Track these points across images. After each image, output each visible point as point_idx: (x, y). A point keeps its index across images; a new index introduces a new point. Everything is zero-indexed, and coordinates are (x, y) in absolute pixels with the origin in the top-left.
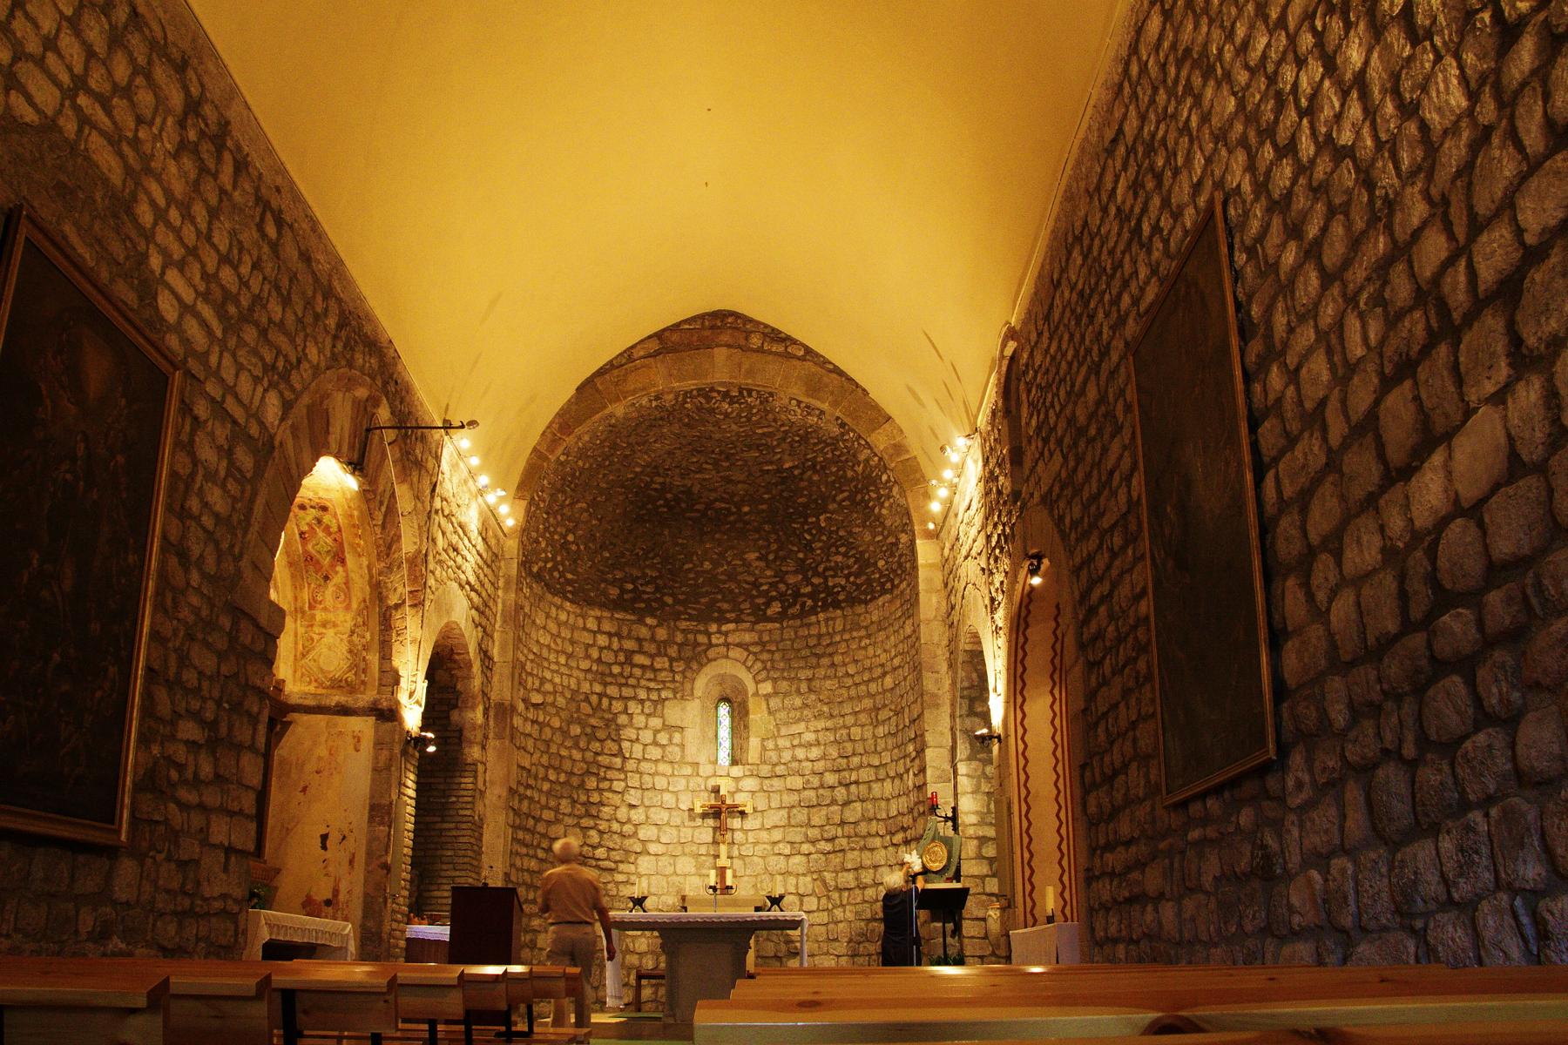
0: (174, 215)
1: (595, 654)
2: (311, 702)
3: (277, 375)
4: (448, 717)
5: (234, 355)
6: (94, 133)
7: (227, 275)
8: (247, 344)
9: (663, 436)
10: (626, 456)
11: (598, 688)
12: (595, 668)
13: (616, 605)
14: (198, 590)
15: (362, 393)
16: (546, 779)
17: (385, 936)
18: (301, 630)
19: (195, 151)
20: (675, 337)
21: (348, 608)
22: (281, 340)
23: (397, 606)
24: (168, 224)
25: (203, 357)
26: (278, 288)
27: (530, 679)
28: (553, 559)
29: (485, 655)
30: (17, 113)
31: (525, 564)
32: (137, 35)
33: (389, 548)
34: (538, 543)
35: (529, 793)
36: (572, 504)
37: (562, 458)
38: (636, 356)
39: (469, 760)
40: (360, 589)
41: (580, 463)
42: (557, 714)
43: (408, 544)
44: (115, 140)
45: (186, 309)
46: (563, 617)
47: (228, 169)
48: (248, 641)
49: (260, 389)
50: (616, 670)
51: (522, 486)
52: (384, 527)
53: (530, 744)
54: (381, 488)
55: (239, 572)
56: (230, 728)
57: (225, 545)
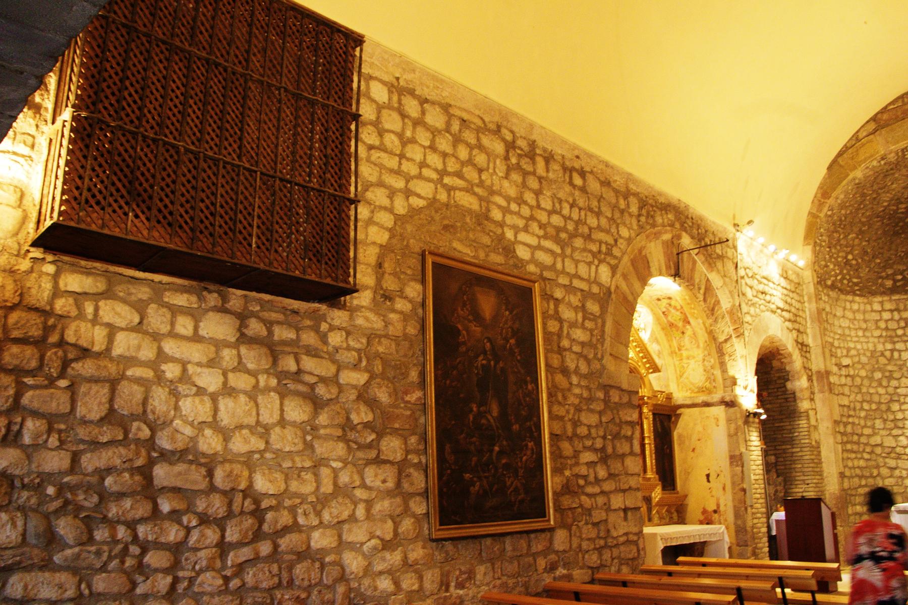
0: (514, 207)
1: (882, 325)
2: (688, 402)
3: (603, 255)
4: (785, 386)
5: (571, 257)
6: (457, 192)
7: (556, 220)
8: (577, 249)
9: (896, 179)
10: (875, 199)
11: (889, 346)
12: (884, 334)
13: (893, 290)
14: (578, 385)
15: (667, 237)
16: (862, 409)
17: (749, 529)
18: (677, 363)
19: (518, 167)
20: (885, 116)
21: (698, 347)
22: (601, 236)
23: (726, 341)
24: (511, 213)
25: (553, 267)
26: (591, 210)
27: (839, 351)
28: (841, 273)
29: (803, 347)
30: (415, 206)
31: (821, 282)
32: (467, 131)
33: (713, 310)
34: (827, 266)
35: (851, 420)
36: (846, 237)
37: (829, 213)
38: (861, 136)
39: (802, 410)
40: (703, 336)
41: (843, 212)
42: (863, 368)
43: (726, 304)
44: (469, 190)
45: (533, 248)
46: (855, 307)
47: (540, 163)
48: (617, 399)
49: (593, 268)
50: (900, 332)
51: (806, 237)
52: (705, 300)
53: (846, 390)
54: (697, 281)
55: (603, 367)
56: (614, 448)
57: (591, 356)
